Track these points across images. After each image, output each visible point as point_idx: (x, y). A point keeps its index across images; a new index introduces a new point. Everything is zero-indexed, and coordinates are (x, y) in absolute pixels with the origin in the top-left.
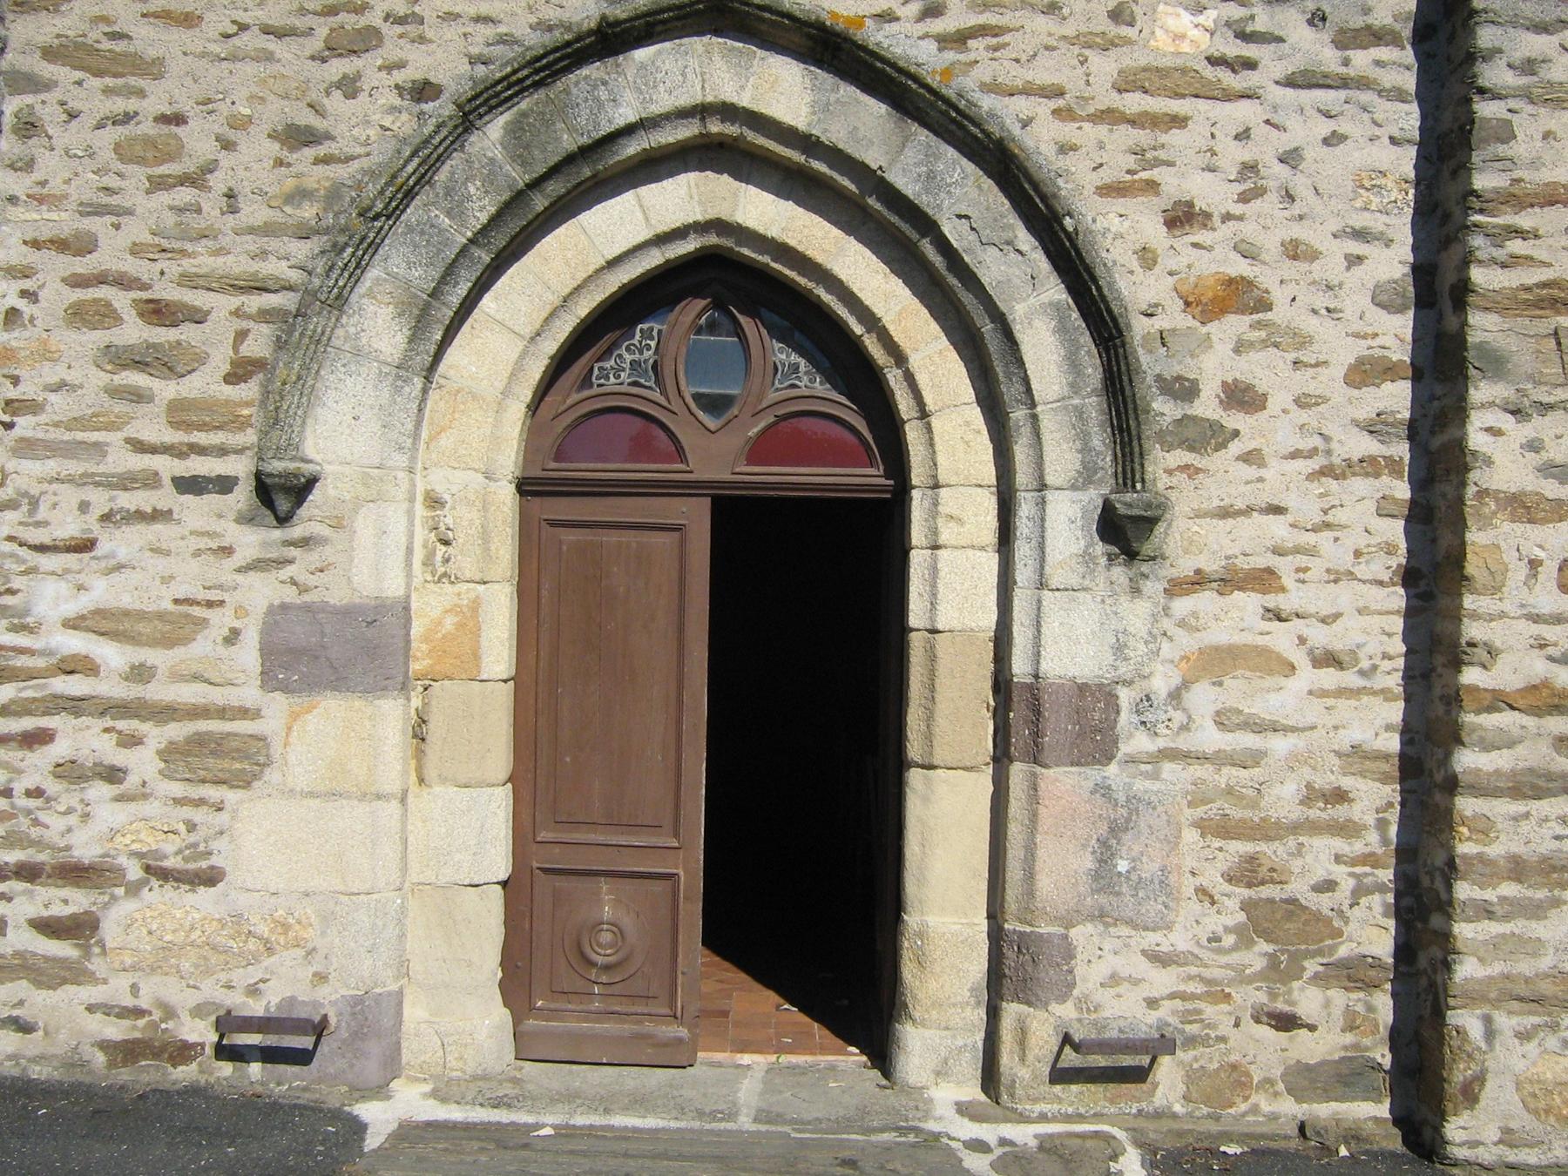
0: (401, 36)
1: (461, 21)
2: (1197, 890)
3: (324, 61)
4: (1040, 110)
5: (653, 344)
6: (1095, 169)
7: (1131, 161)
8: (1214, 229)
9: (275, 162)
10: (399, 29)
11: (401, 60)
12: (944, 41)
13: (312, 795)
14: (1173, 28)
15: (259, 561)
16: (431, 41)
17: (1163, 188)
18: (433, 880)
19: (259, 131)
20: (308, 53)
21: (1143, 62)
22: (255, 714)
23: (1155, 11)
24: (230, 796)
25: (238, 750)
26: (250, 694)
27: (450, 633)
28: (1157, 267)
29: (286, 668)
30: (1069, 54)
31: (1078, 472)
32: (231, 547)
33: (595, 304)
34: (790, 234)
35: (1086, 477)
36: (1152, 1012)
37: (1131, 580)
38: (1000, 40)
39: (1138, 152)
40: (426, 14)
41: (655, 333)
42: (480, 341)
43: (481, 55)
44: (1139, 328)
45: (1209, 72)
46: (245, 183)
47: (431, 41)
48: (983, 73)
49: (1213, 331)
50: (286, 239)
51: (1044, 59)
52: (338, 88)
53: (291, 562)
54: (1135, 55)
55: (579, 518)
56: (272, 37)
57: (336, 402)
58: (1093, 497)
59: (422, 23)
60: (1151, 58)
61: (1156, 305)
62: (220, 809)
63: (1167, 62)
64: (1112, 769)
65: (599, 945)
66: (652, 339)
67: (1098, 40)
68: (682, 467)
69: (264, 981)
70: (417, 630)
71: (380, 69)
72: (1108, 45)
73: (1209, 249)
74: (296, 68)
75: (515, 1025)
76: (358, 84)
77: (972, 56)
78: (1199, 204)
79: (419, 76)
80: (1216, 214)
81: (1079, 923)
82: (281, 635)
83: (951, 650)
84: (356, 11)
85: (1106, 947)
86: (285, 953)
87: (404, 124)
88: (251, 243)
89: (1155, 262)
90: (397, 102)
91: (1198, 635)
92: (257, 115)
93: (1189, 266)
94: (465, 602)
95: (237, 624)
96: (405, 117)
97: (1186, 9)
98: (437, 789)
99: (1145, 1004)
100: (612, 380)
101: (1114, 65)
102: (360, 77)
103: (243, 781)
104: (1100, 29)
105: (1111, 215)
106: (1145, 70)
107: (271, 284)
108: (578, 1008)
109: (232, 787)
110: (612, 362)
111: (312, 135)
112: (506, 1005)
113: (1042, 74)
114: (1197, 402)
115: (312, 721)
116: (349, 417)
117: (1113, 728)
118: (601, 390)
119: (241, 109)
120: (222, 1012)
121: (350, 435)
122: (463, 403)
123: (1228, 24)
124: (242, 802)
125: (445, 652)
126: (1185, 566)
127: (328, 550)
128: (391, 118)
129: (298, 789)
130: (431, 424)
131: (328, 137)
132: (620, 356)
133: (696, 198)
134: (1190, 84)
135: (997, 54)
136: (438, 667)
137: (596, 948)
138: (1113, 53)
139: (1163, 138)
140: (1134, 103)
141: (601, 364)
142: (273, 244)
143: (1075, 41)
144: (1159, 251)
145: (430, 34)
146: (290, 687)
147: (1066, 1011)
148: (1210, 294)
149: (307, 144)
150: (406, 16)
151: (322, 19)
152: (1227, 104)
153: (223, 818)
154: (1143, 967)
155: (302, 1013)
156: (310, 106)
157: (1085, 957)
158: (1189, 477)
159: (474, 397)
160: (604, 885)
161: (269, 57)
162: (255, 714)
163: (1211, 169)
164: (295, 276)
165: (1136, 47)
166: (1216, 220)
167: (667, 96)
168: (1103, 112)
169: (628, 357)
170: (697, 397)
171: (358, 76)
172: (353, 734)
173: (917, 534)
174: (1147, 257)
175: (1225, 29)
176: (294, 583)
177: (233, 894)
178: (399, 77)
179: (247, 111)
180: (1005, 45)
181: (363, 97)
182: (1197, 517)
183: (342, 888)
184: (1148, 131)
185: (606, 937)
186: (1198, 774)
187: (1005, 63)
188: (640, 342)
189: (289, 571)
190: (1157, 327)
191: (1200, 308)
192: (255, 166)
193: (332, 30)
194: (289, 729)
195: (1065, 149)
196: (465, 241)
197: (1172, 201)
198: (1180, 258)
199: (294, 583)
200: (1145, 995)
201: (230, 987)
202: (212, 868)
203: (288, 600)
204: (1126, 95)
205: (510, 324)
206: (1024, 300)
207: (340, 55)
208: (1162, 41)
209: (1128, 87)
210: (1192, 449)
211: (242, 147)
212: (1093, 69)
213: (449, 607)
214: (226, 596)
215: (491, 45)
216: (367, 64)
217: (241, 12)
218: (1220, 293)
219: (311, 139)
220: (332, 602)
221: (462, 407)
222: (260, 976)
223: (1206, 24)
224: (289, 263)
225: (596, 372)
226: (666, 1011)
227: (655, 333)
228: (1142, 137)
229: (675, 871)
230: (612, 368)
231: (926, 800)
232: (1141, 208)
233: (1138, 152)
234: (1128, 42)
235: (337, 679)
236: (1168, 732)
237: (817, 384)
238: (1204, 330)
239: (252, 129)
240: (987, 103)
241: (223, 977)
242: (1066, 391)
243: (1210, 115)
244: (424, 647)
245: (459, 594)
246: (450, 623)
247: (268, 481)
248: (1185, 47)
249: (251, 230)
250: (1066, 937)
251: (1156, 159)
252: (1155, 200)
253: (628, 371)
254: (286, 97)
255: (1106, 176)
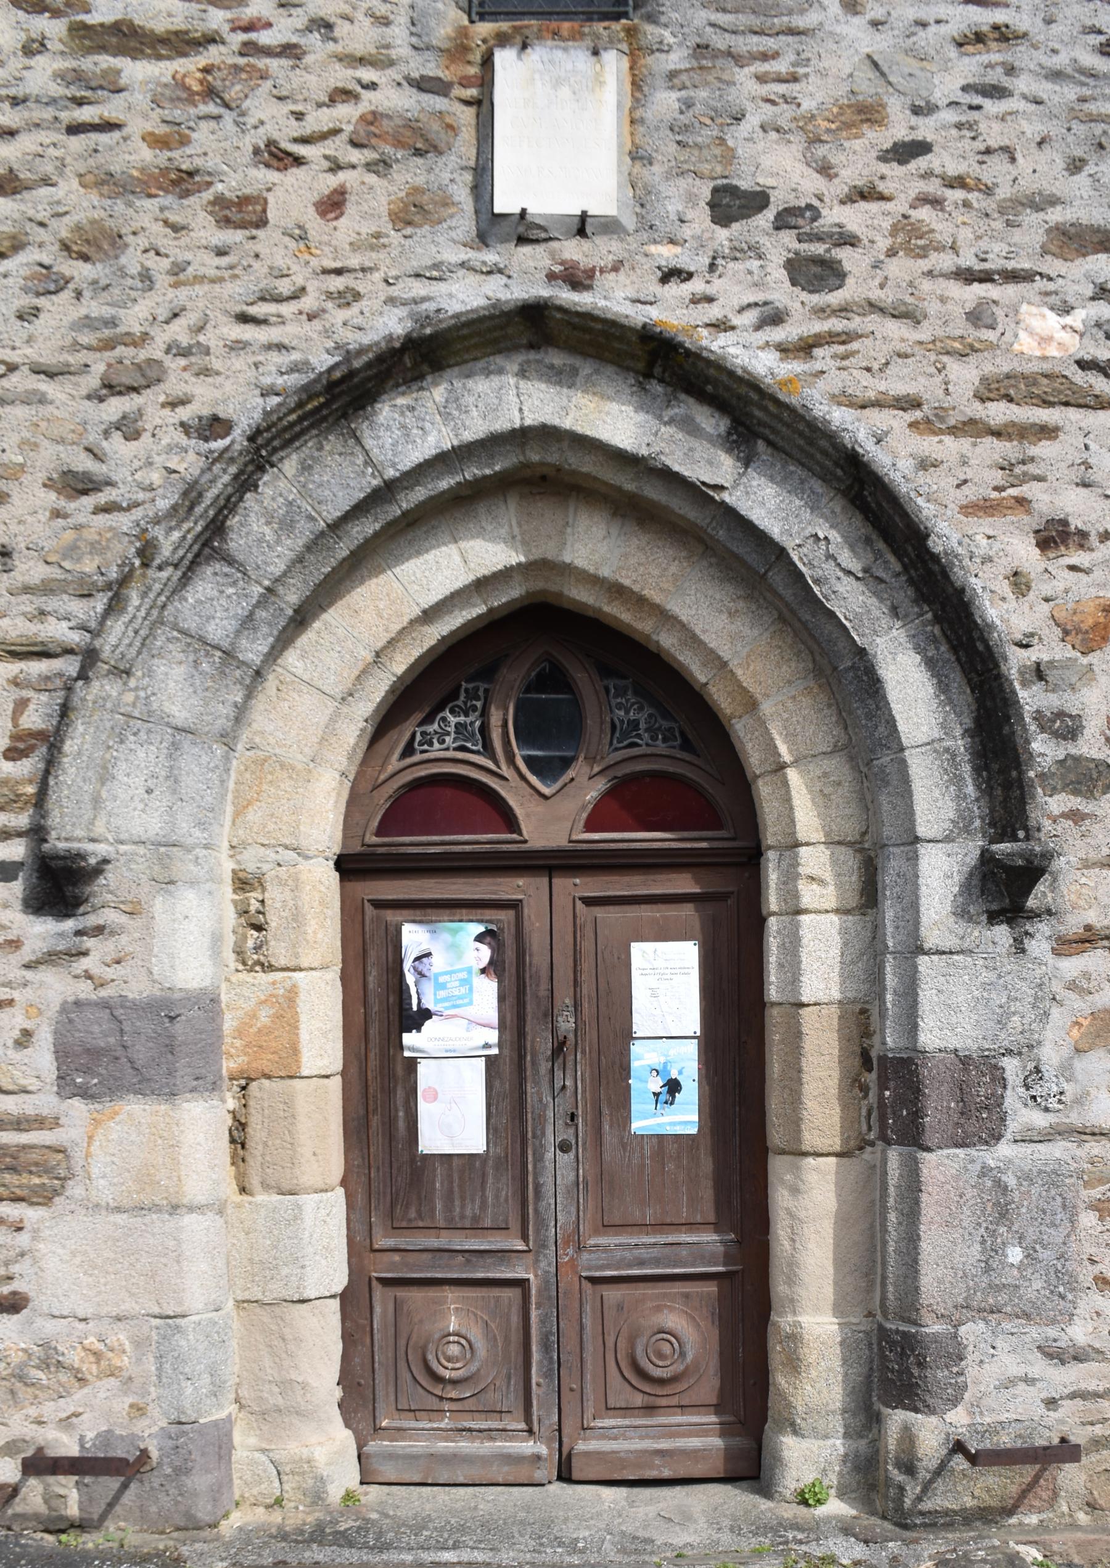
0: (185, 369)
1: (249, 349)
2: (1096, 1279)
3: (101, 400)
4: (895, 424)
5: (479, 704)
6: (958, 486)
7: (998, 478)
8: (1092, 550)
9: (52, 513)
10: (183, 362)
11: (185, 394)
12: (785, 350)
13: (118, 1210)
14: (1038, 330)
15: (50, 954)
16: (218, 373)
17: (1035, 505)
18: (260, 1296)
19: (33, 481)
20: (84, 392)
21: (1006, 369)
22: (54, 1123)
23: (1017, 312)
24: (30, 1214)
25: (37, 1164)
26: (45, 1102)
27: (265, 1026)
28: (1031, 593)
29: (87, 1071)
30: (925, 362)
31: (953, 822)
32: (18, 941)
33: (413, 659)
34: (624, 573)
35: (961, 827)
36: (1051, 1413)
37: (1015, 940)
38: (849, 347)
39: (1006, 467)
40: (212, 344)
41: (481, 693)
42: (286, 704)
43: (273, 385)
44: (1015, 661)
45: (1080, 378)
46: (20, 538)
47: (218, 373)
48: (834, 381)
49: (1095, 661)
50: (65, 597)
51: (897, 368)
52: (118, 429)
53: (85, 954)
54: (998, 361)
55: (407, 897)
56: (42, 376)
57: (128, 775)
58: (970, 850)
59: (208, 353)
60: (1015, 364)
61: (1032, 635)
62: (19, 1229)
63: (1034, 367)
64: (1005, 1149)
65: (449, 1360)
66: (478, 699)
67: (957, 345)
68: (515, 836)
69: (77, 1415)
70: (229, 1023)
71: (163, 406)
72: (967, 351)
73: (1087, 572)
74: (70, 409)
75: (360, 1448)
76: (140, 423)
77: (818, 366)
78: (1075, 523)
79: (206, 412)
80: (1093, 533)
81: (969, 1320)
82: (77, 1035)
83: (817, 1025)
84: (135, 344)
85: (999, 1344)
86: (99, 1383)
87: (189, 464)
88: (28, 603)
89: (1029, 588)
90: (184, 440)
91: (1090, 998)
92: (29, 463)
93: (1067, 591)
94: (281, 992)
95: (28, 1025)
96: (191, 456)
97: (1052, 309)
98: (261, 1198)
99: (1043, 1406)
100: (436, 745)
101: (975, 372)
102: (141, 415)
103: (44, 1197)
104: (958, 333)
105: (978, 537)
106: (1008, 376)
107: (52, 647)
108: (429, 1425)
109: (32, 1204)
110: (436, 726)
111: (91, 481)
112: (347, 1425)
113: (897, 385)
114: (1080, 741)
115: (115, 1130)
116: (142, 791)
117: (1000, 1105)
118: (426, 756)
119: (13, 457)
120: (29, 1453)
121: (143, 811)
122: (271, 773)
123: (1098, 325)
124: (42, 1220)
125: (260, 1047)
126: (1073, 924)
127: (124, 939)
128: (176, 459)
129: (103, 1204)
130: (236, 797)
131: (110, 483)
132: (444, 719)
133: (519, 538)
134: (1060, 392)
135: (845, 363)
136: (254, 1065)
137: (446, 1364)
138: (972, 359)
139: (1033, 451)
140: (998, 412)
141: (423, 728)
142: (51, 603)
143: (931, 346)
144: (1033, 576)
145: (216, 364)
146: (90, 1092)
147: (958, 1418)
148: (1090, 622)
149: (85, 492)
150: (190, 347)
151: (98, 355)
152: (1100, 413)
153: (23, 1239)
154: (1039, 1367)
155: (119, 1452)
156: (88, 450)
157: (977, 1356)
158: (1076, 823)
159: (283, 766)
160: (450, 1294)
161: (43, 400)
162: (54, 1123)
163: (1086, 485)
164: (76, 638)
165: (998, 352)
166: (1094, 539)
167: (481, 422)
168: (964, 423)
169: (453, 720)
170: (529, 761)
171: (140, 413)
172: (160, 1141)
173: (773, 901)
174: (1019, 581)
175: (1095, 330)
176: (88, 976)
177: (39, 1322)
178: (184, 413)
179: (20, 459)
180: (853, 354)
181: (146, 437)
182: (1087, 867)
183: (156, 1310)
184: (1015, 443)
185: (454, 1350)
186: (1095, 1152)
187: (855, 372)
188: (465, 703)
189: (85, 963)
190: (1034, 659)
191: (1080, 637)
192: (29, 519)
193: (109, 365)
194: (90, 1138)
195: (925, 464)
196: (261, 590)
197: (1044, 520)
198: (1055, 582)
199: (88, 976)
200: (1044, 1395)
201: (40, 1423)
202: (14, 1293)
203: (82, 996)
204: (989, 404)
205: (319, 684)
206: (887, 633)
207: (120, 393)
208: (1026, 344)
209: (991, 395)
210: (1076, 792)
211: (15, 499)
212: (951, 377)
213: (263, 998)
214: (16, 995)
215: (286, 373)
216: (149, 401)
217: (8, 351)
218: (1102, 620)
219: (90, 486)
220: (131, 996)
221: (270, 777)
222: (72, 1409)
223: (1074, 325)
224: (71, 624)
225: (418, 738)
226: (522, 1426)
227: (481, 693)
228: (1008, 449)
229: (526, 1276)
230: (436, 732)
231: (795, 1191)
232: (1012, 528)
233: (1006, 467)
234: (992, 347)
235: (140, 1082)
236: (1061, 1107)
237: (659, 742)
238: (1085, 661)
239: (26, 479)
240: (839, 417)
241: (32, 1411)
242: (937, 733)
243: (1083, 425)
244: (238, 1043)
245: (274, 983)
246: (264, 1017)
247: (53, 864)
248: (1053, 351)
249: (27, 589)
250: (955, 1336)
251: (1025, 474)
252: (1026, 519)
253: (453, 735)
254: (61, 441)
255: (970, 493)
